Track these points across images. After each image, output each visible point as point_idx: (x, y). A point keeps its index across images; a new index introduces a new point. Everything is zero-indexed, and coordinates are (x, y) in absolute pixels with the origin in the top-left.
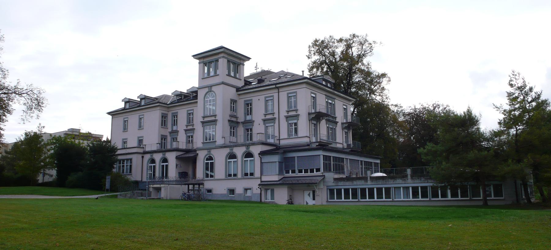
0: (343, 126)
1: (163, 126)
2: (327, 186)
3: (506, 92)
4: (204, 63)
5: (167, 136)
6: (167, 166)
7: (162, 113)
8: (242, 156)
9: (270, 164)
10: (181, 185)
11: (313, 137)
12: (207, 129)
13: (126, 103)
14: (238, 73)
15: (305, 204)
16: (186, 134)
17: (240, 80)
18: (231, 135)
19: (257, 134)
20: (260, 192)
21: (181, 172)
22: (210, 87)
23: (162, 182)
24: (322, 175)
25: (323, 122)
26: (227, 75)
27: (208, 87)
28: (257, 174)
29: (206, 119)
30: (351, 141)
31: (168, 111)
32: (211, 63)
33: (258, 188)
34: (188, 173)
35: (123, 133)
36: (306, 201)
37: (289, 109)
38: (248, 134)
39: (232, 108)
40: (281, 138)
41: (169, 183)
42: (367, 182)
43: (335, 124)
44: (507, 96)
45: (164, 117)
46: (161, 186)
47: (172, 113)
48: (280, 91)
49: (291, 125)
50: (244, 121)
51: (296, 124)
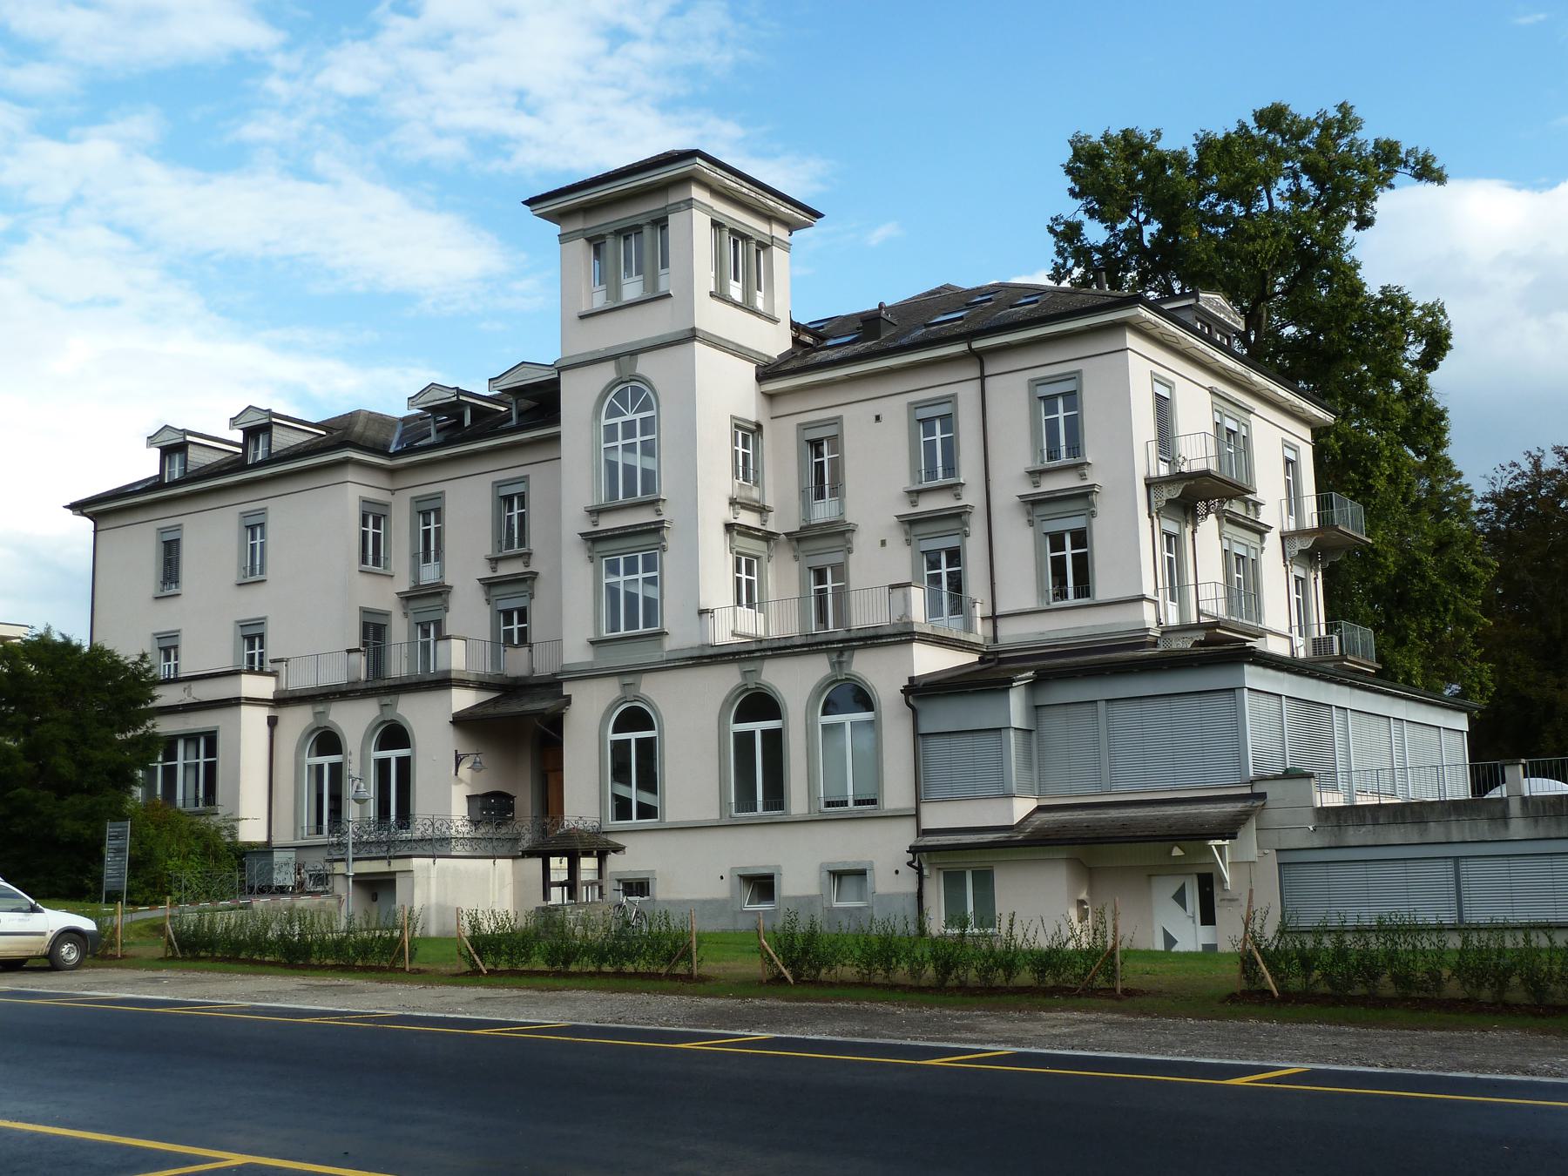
0: (1287, 549)
1: (370, 566)
2: (1277, 850)
3: (65, 507)
4: (589, 240)
5: (387, 614)
6: (405, 765)
7: (365, 501)
8: (810, 709)
9: (967, 741)
10: (493, 857)
11: (1168, 602)
12: (618, 574)
13: (167, 452)
14: (759, 289)
15: (1159, 945)
16: (488, 601)
17: (775, 321)
18: (739, 603)
19: (892, 587)
20: (915, 889)
21: (480, 792)
22: (625, 356)
23: (391, 849)
24: (1247, 791)
25: (1209, 526)
26: (712, 294)
27: (615, 357)
28: (897, 792)
29: (608, 523)
30: (1319, 629)
31: (393, 492)
32: (626, 238)
33: (910, 864)
34: (512, 798)
35: (237, 588)
36: (1165, 932)
37: (500, 551)
38: (820, 591)
39: (741, 463)
40: (999, 611)
41: (437, 846)
42: (1506, 825)
43: (1256, 537)
44: (1262, 507)
45: (374, 515)
46: (393, 869)
47: (416, 500)
48: (99, 528)
49: (1057, 541)
50: (413, 589)
51: (1080, 538)
